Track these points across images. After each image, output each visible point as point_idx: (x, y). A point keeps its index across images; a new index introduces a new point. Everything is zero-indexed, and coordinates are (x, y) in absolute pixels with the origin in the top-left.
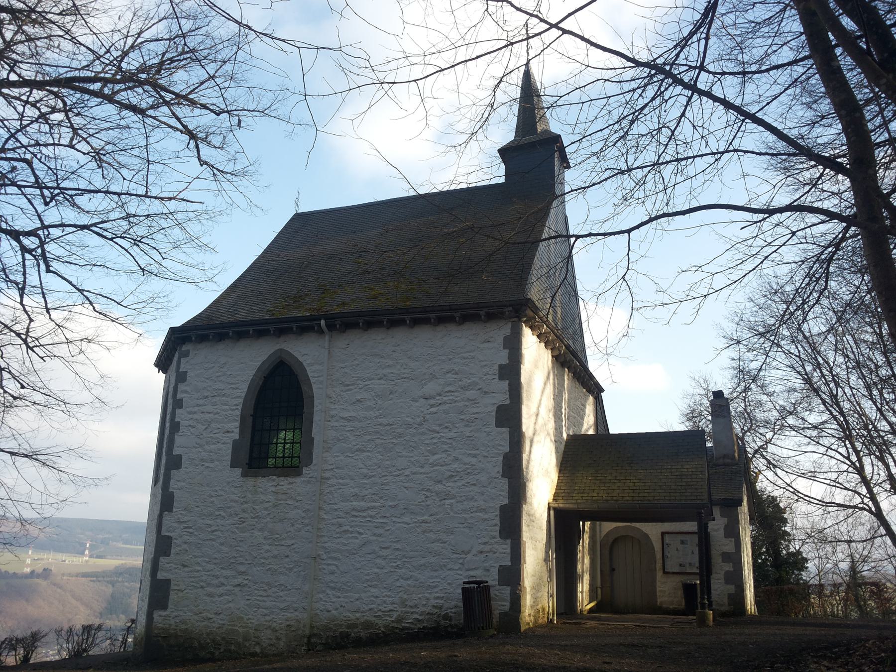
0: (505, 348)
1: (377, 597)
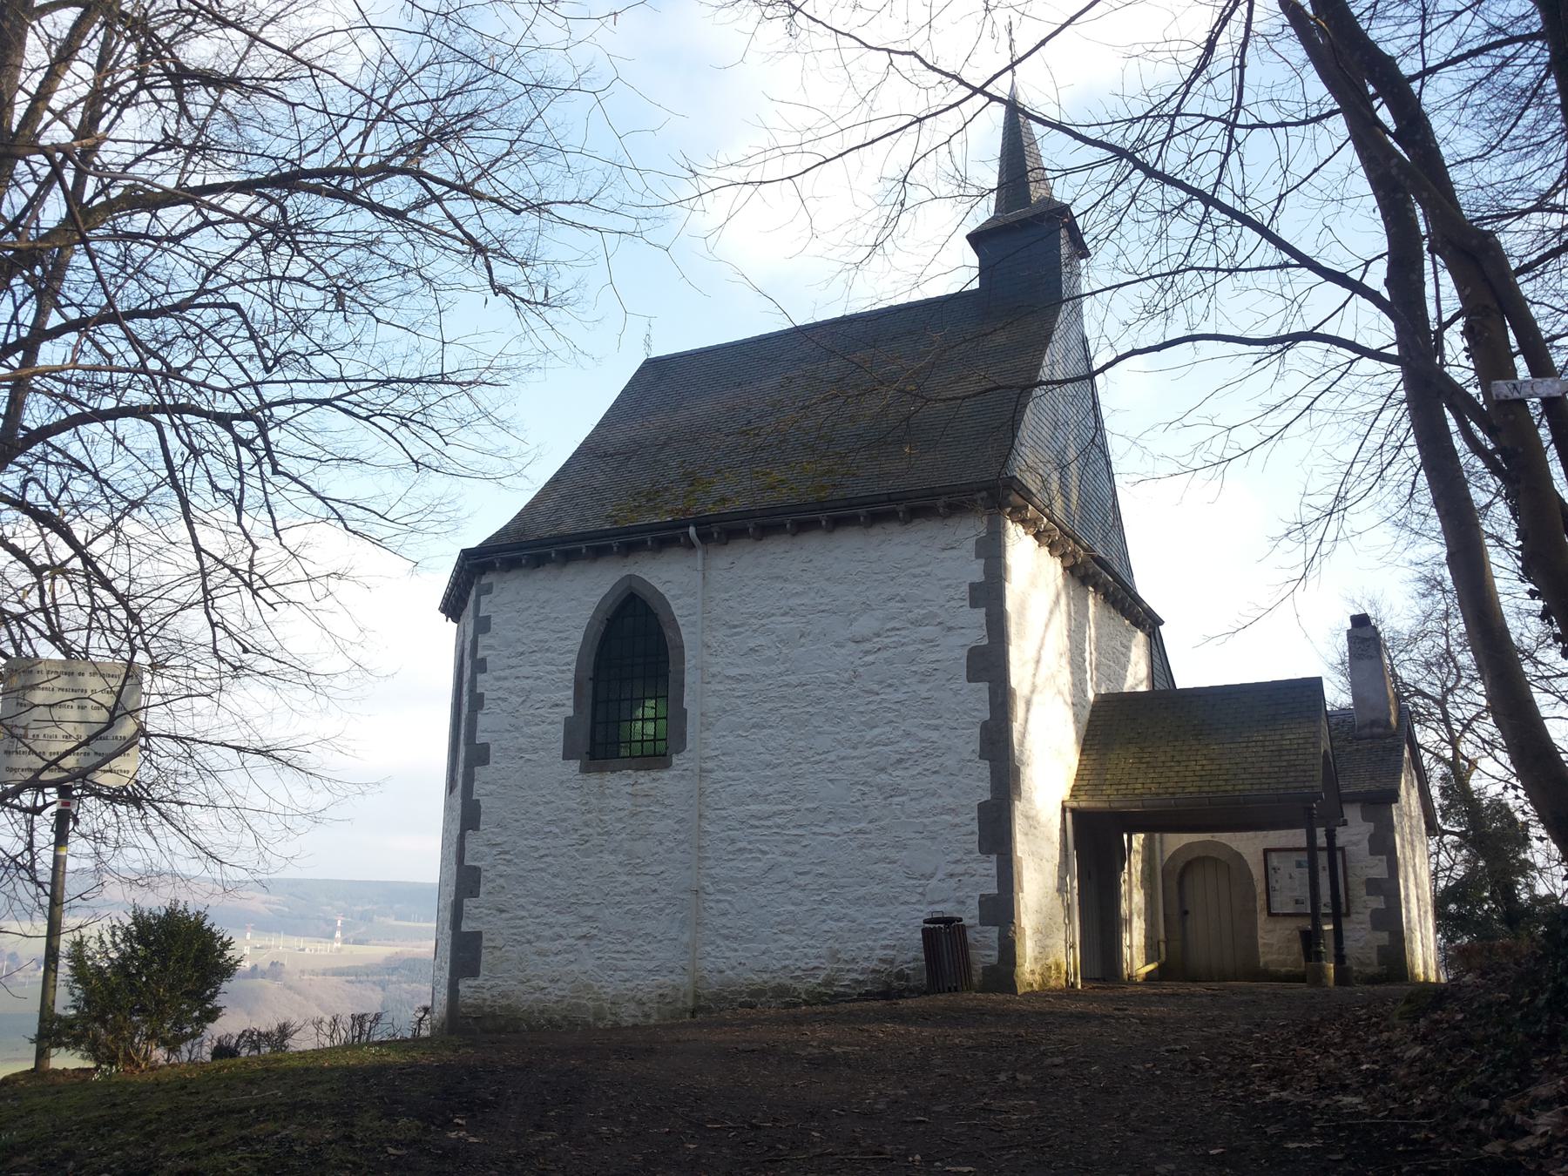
0: (978, 556)
1: (793, 948)
